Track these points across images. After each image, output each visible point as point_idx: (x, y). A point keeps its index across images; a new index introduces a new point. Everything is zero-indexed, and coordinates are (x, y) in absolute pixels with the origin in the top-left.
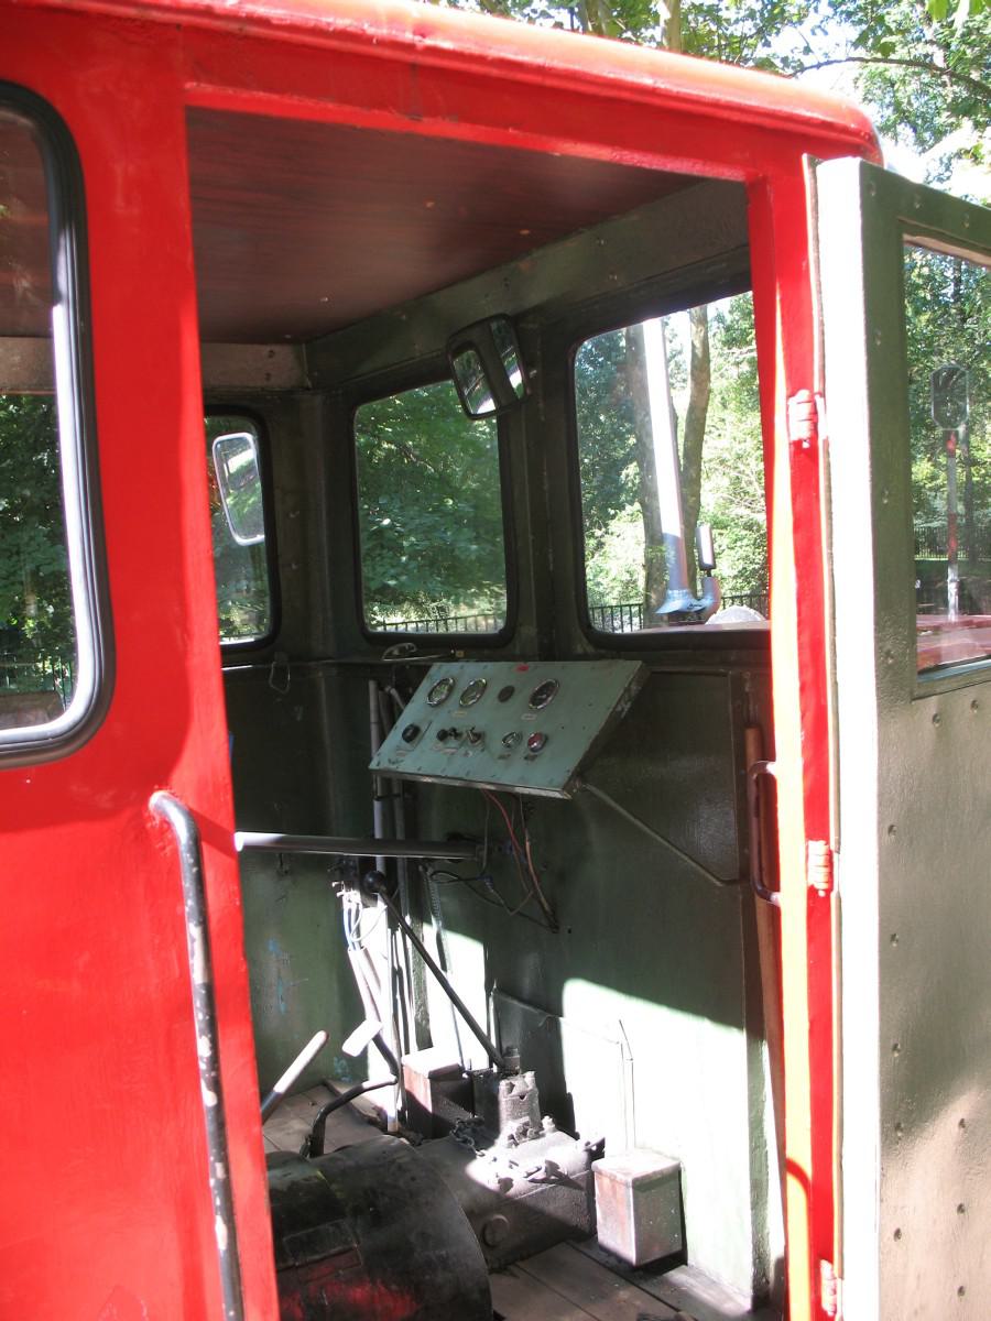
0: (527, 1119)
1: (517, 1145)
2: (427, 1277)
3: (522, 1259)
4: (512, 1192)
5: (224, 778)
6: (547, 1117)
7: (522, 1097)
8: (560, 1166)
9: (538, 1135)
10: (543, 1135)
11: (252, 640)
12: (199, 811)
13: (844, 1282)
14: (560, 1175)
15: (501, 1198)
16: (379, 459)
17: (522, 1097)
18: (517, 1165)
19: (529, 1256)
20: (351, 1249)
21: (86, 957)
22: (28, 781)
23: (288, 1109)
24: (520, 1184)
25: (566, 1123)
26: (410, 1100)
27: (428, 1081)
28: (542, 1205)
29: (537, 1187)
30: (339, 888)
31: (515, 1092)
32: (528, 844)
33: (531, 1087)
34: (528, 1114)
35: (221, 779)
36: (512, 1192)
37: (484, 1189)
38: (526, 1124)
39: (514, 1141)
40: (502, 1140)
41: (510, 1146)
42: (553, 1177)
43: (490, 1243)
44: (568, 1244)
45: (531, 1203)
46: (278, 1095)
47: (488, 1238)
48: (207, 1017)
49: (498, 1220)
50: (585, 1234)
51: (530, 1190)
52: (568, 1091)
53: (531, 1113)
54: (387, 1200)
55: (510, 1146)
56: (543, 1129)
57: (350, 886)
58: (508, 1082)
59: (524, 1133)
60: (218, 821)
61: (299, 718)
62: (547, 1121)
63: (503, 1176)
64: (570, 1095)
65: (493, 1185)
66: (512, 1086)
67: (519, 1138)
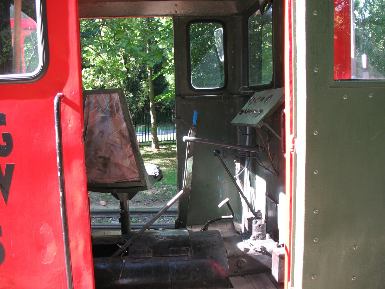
0: (260, 233)
1: (255, 240)
2: (209, 269)
3: (250, 274)
4: (248, 253)
5: (77, 91)
6: (268, 234)
7: (260, 226)
8: (267, 249)
9: (263, 239)
10: (266, 239)
11: (218, 88)
12: (70, 99)
13: (294, 288)
14: (266, 251)
15: (245, 254)
16: (257, 31)
17: (260, 226)
18: (253, 245)
19: (253, 274)
20: (188, 256)
21: (38, 134)
22: (24, 87)
23: (219, 226)
24: (251, 251)
25: (275, 237)
26: (158, 201)
27: (247, 220)
28: (258, 259)
29: (257, 253)
30: (236, 162)
31: (258, 224)
32: (269, 147)
33: (263, 223)
34: (261, 232)
35: (77, 91)
36: (248, 253)
37: (239, 250)
38: (260, 234)
39: (255, 239)
40: (252, 237)
41: (253, 240)
42: (264, 252)
43: (239, 266)
44: (267, 273)
45: (255, 258)
46: (168, 206)
47: (239, 265)
48: (58, 152)
49: (243, 260)
50: (268, 271)
51: (255, 254)
52: (278, 228)
53: (262, 231)
54: (204, 245)
55: (253, 240)
56: (266, 237)
57: (238, 162)
58: (255, 220)
59: (258, 237)
60: (75, 102)
61: (232, 112)
62: (268, 235)
63: (247, 247)
64: (278, 229)
65: (242, 250)
66: (257, 222)
67: (257, 238)
